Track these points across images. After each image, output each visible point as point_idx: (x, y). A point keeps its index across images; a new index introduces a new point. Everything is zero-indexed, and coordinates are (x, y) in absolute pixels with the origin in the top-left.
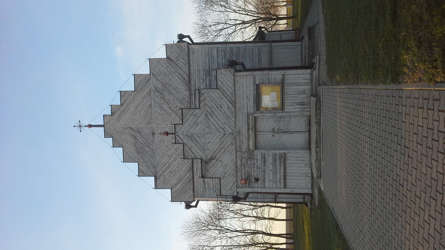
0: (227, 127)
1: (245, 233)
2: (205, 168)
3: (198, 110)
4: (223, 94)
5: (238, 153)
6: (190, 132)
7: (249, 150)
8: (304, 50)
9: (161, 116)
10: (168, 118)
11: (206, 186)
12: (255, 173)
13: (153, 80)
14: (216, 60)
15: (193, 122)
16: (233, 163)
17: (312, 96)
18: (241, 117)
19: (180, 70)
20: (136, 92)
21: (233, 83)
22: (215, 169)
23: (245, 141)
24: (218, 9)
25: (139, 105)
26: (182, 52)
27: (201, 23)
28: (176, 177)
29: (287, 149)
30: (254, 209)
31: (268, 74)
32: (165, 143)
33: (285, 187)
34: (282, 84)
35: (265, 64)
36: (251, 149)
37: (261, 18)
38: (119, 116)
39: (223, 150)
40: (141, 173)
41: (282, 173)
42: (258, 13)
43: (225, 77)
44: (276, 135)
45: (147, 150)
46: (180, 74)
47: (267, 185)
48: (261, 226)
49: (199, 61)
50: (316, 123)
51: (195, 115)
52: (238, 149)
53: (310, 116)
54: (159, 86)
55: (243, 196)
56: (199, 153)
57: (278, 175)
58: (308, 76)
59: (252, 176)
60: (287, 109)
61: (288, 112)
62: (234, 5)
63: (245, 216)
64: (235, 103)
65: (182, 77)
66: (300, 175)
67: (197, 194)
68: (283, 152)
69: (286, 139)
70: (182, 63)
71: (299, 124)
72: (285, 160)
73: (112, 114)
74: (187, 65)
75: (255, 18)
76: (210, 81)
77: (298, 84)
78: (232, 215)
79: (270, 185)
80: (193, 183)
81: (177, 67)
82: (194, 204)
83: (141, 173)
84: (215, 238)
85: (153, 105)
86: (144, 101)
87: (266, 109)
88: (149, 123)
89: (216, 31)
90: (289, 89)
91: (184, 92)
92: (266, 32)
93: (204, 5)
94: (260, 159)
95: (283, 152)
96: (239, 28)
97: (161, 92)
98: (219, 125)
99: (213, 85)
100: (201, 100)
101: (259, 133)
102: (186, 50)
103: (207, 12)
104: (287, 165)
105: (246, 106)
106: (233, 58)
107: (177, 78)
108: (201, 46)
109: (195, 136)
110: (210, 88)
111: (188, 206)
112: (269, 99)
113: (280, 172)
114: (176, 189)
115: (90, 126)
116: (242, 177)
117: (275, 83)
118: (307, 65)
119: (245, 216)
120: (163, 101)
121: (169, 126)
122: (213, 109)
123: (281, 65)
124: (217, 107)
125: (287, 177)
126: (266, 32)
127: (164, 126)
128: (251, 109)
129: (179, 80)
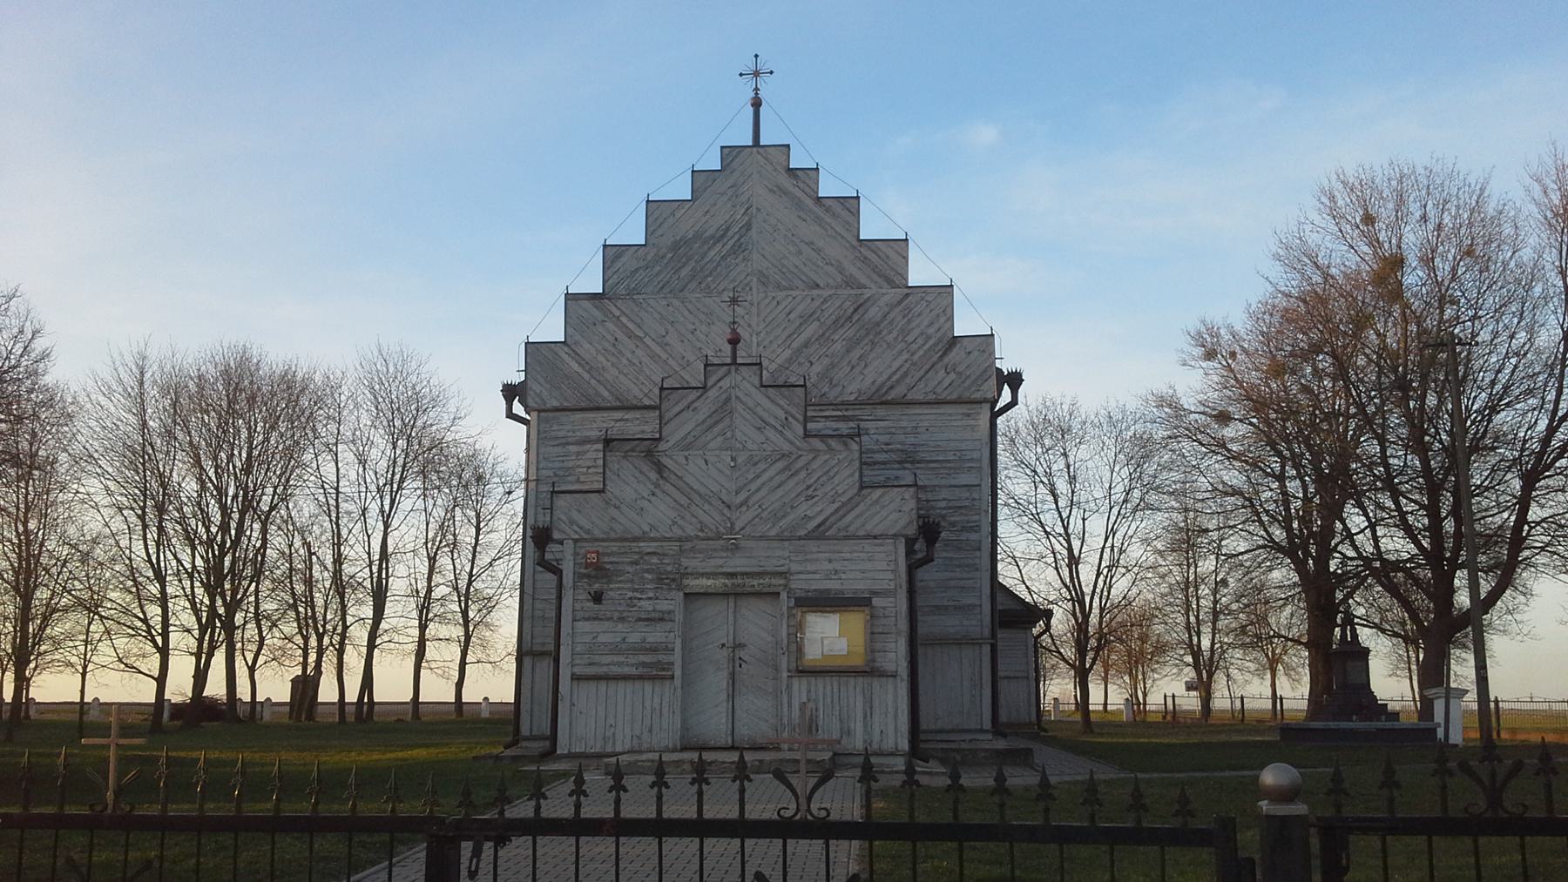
0: (750, 514)
1: (381, 560)
2: (632, 450)
3: (801, 431)
4: (844, 504)
5: (675, 546)
6: (740, 407)
7: (684, 575)
8: (968, 737)
9: (783, 315)
10: (776, 338)
11: (573, 448)
12: (616, 592)
13: (891, 295)
14: (944, 482)
15: (765, 416)
16: (647, 529)
17: (835, 754)
18: (779, 553)
19: (919, 375)
20: (855, 243)
21: (877, 531)
22: (630, 482)
23: (711, 565)
24: (1117, 479)
25: (818, 251)
26: (968, 382)
27: (1076, 426)
28: (601, 358)
29: (687, 682)
30: (456, 589)
31: (898, 633)
32: (704, 328)
33: (576, 678)
34: (871, 671)
35: (930, 625)
36: (686, 582)
37: (1086, 616)
38: (785, 193)
39: (684, 501)
40: (613, 255)
41: (616, 670)
42: (1102, 610)
43: (894, 511)
44: (725, 652)
45: (684, 273)
46: (906, 374)
47: (583, 626)
48: (400, 614)
49: (945, 431)
50: (761, 761)
51: (786, 423)
52: (688, 545)
53: (778, 749)
54: (874, 313)
55: (548, 556)
56: (677, 432)
57: (609, 659)
58: (889, 745)
59: (609, 582)
60: (800, 688)
61: (789, 687)
62: (1130, 533)
63: (432, 560)
64: (817, 538)
65: (898, 381)
66: (611, 721)
67: (547, 421)
68: (678, 673)
69: (715, 683)
70: (940, 381)
71: (757, 717)
72: (653, 678)
73: (792, 172)
74: (932, 397)
75: (1087, 599)
76: (884, 463)
77: (868, 715)
78: (439, 513)
79: (583, 635)
80: (582, 410)
81: (927, 367)
82: (518, 409)
83: (613, 255)
84: (363, 462)
85: (815, 292)
86: (829, 269)
87: (800, 627)
88: (764, 280)
89: (1049, 475)
90: (853, 693)
91: (853, 387)
92: (1035, 631)
93: (1130, 433)
94: (659, 608)
95: (678, 673)
96: (1058, 547)
97: (856, 317)
98: (758, 490)
99: (873, 474)
100: (830, 441)
101: (732, 604)
102: (977, 396)
103: (1110, 442)
104: (638, 684)
105: (810, 567)
106: (948, 532)
107: (896, 365)
108: (986, 439)
109: (727, 421)
110: (862, 464)
111: (510, 392)
112: (829, 636)
113: (620, 664)
114: (566, 357)
115: (757, 104)
116: (609, 555)
117: (873, 651)
118: (922, 745)
119: (432, 560)
120: (829, 322)
121: (755, 340)
122: (803, 474)
123: (921, 669)
124: (808, 487)
125: (603, 685)
126: (1035, 631)
127: (754, 324)
128: (799, 584)
129: (890, 371)
